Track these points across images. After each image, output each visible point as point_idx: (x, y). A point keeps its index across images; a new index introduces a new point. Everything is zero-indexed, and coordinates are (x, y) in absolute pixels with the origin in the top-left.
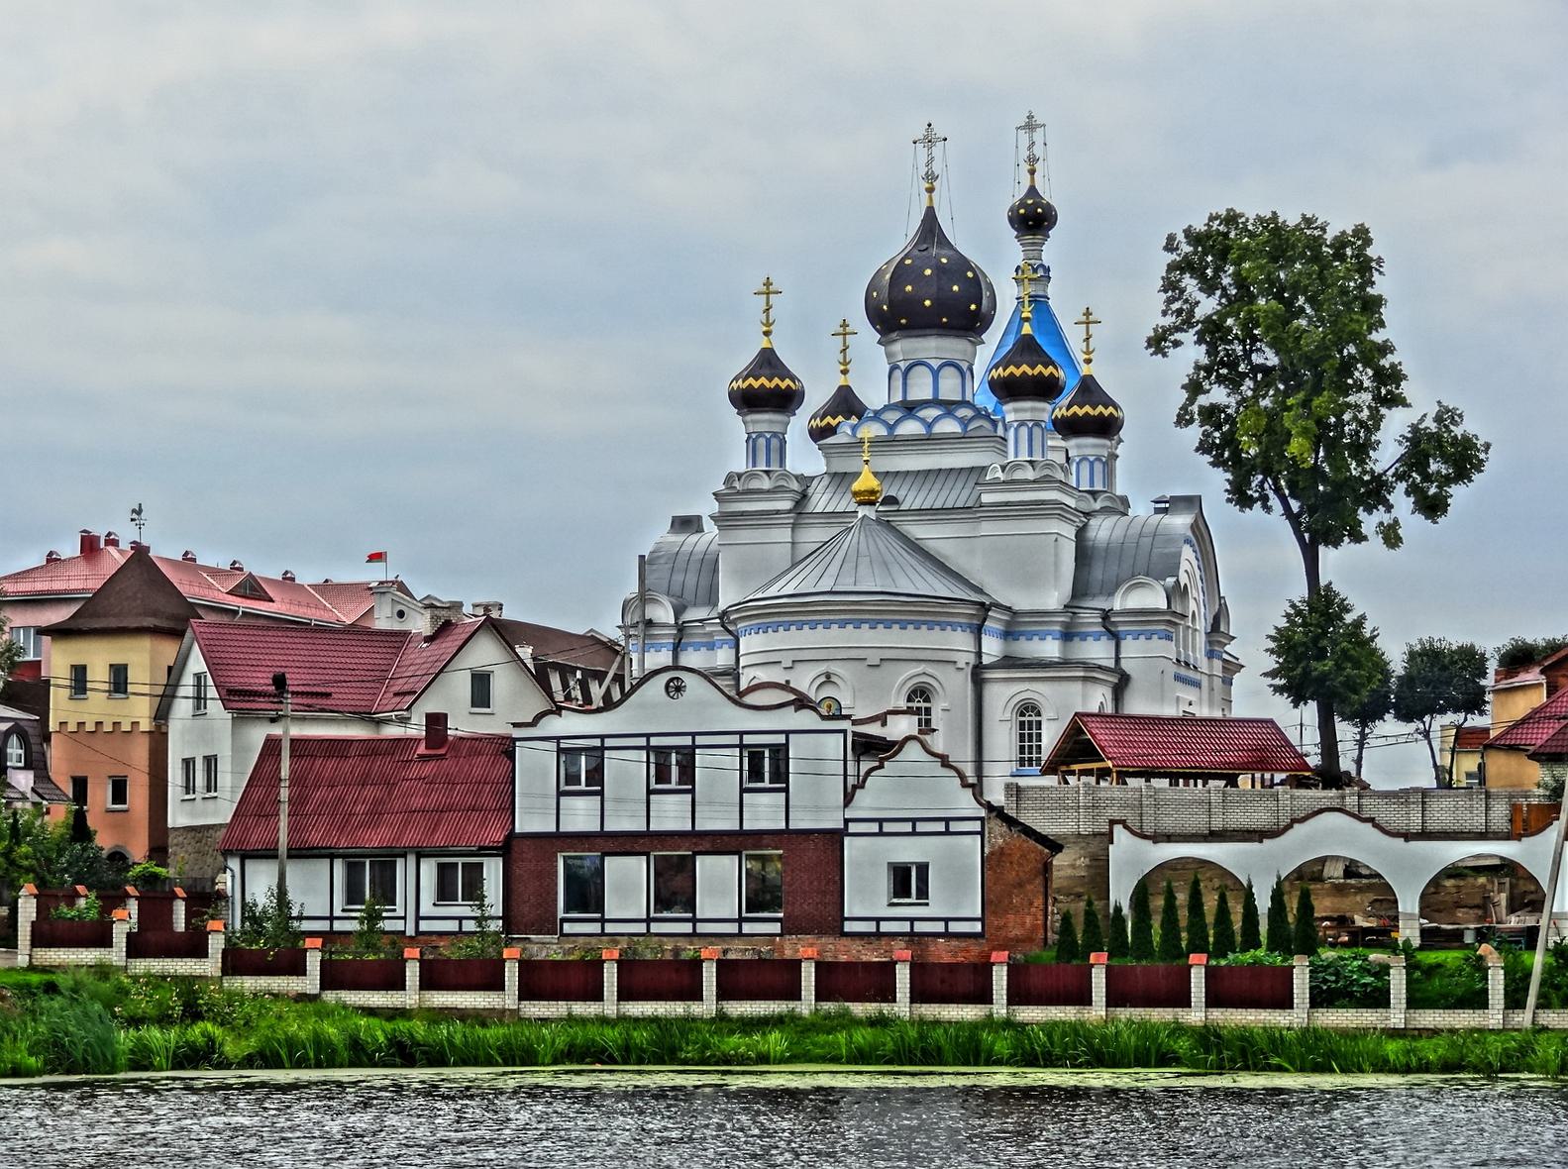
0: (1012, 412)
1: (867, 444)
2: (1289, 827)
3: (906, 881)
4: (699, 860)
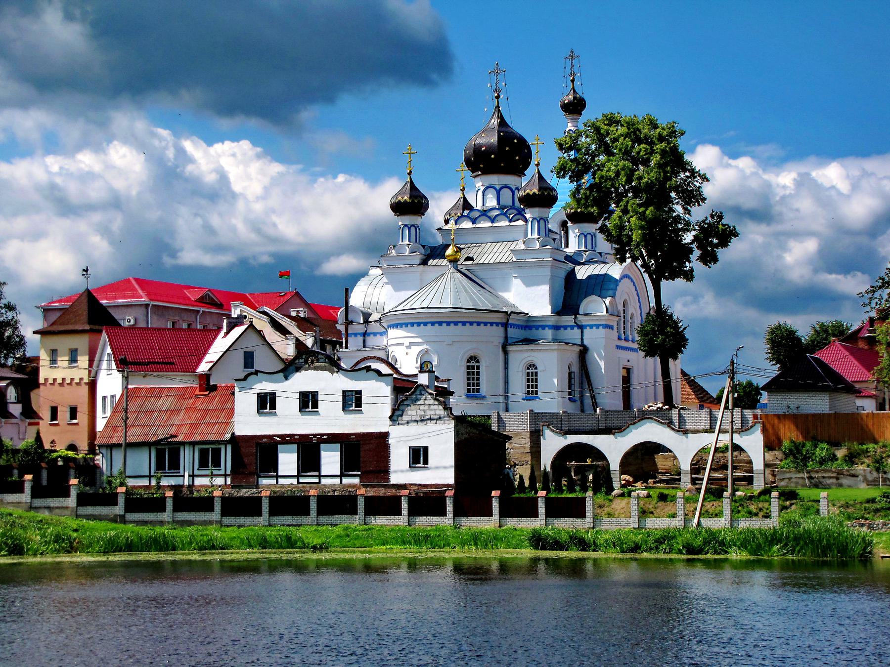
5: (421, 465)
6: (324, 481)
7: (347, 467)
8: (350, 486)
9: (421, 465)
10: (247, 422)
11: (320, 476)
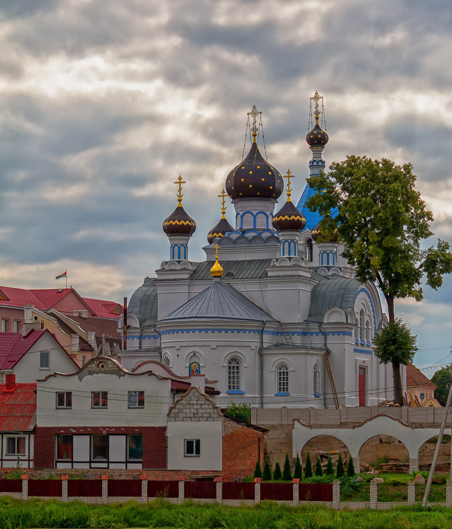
0: (282, 236)
1: (217, 251)
2: (366, 422)
3: (192, 447)
4: (111, 437)
5: (194, 454)
6: (112, 466)
7: (133, 454)
8: (133, 471)
9: (194, 454)
10: (48, 417)
11: (108, 462)
